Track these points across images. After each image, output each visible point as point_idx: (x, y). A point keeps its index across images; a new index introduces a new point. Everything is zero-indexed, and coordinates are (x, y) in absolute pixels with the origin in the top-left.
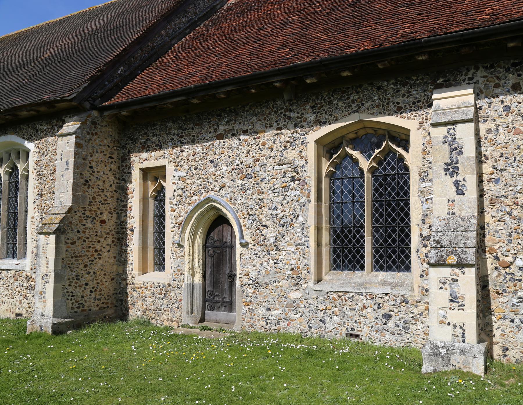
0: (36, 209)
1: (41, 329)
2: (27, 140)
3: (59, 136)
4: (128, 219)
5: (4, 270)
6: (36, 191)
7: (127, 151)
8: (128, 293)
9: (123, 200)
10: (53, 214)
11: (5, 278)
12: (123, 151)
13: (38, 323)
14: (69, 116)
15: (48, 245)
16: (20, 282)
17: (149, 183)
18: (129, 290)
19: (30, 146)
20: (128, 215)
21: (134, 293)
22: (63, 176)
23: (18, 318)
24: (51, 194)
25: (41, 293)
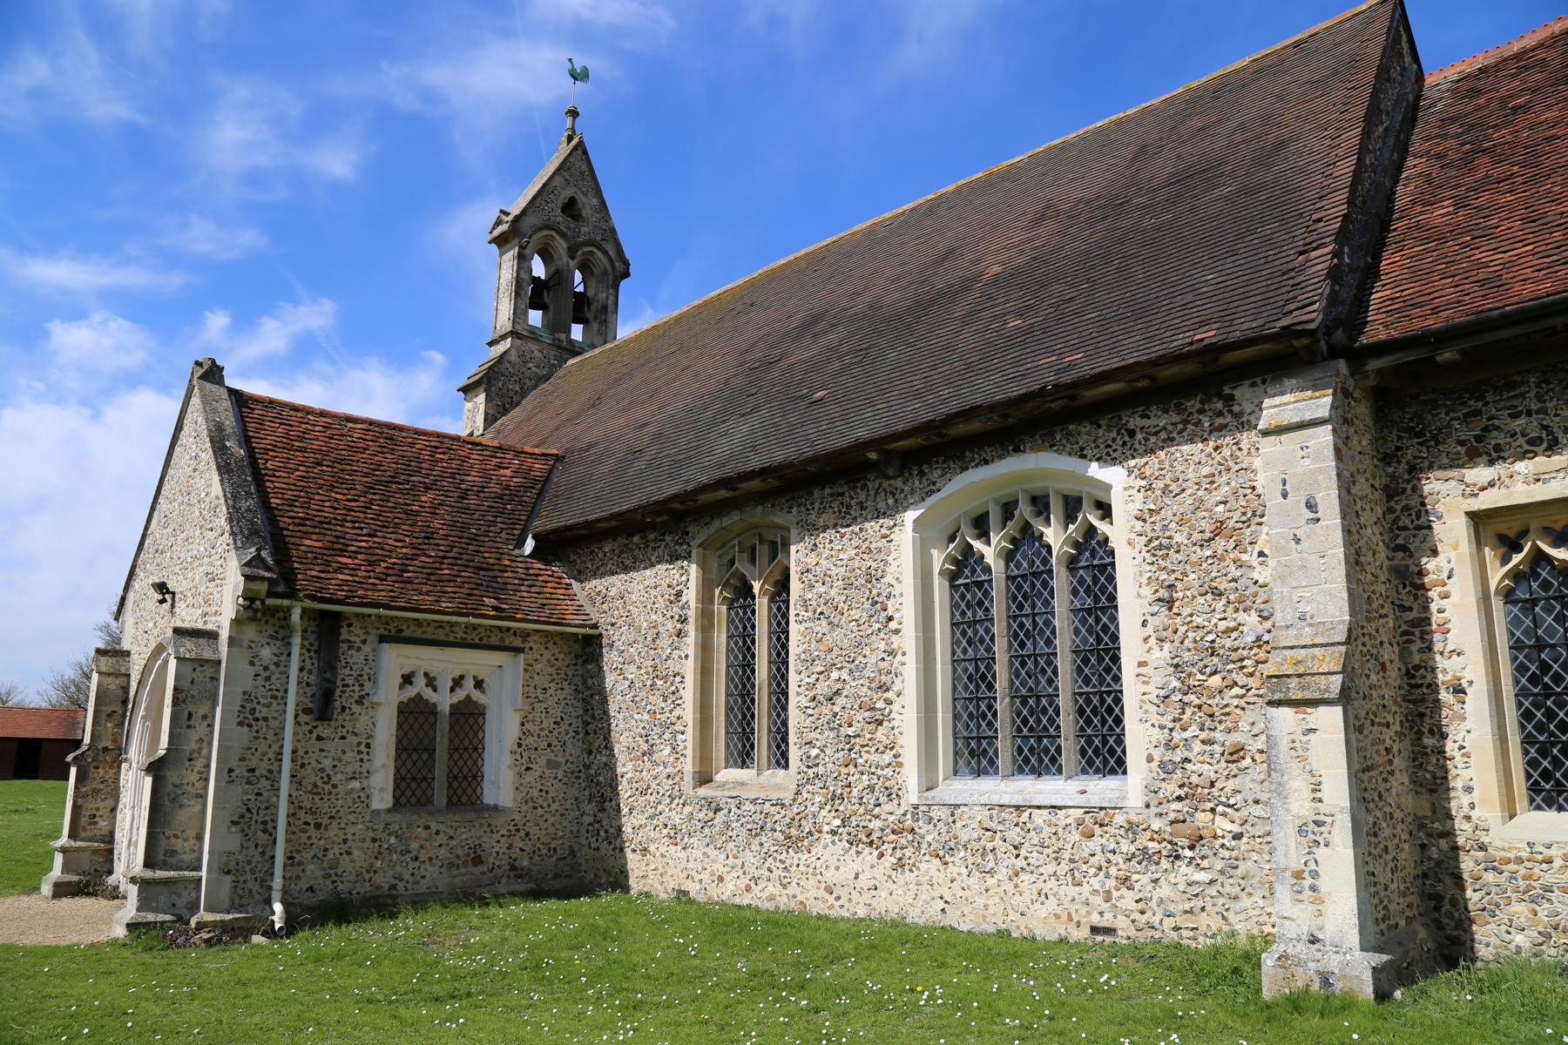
0: (1152, 641)
1: (1326, 982)
2: (1098, 460)
3: (1266, 433)
4: (1438, 657)
5: (1039, 807)
6: (1147, 591)
7: (1403, 466)
8: (1466, 876)
9: (1407, 604)
10: (1292, 648)
11: (1048, 830)
12: (1390, 470)
13: (1312, 965)
14: (1247, 383)
15: (1311, 736)
16: (1104, 841)
17: (1487, 549)
18: (1467, 865)
19: (1113, 477)
20: (1438, 647)
21: (1490, 877)
22: (1298, 541)
23: (1099, 938)
24: (1209, 597)
25: (1298, 875)
